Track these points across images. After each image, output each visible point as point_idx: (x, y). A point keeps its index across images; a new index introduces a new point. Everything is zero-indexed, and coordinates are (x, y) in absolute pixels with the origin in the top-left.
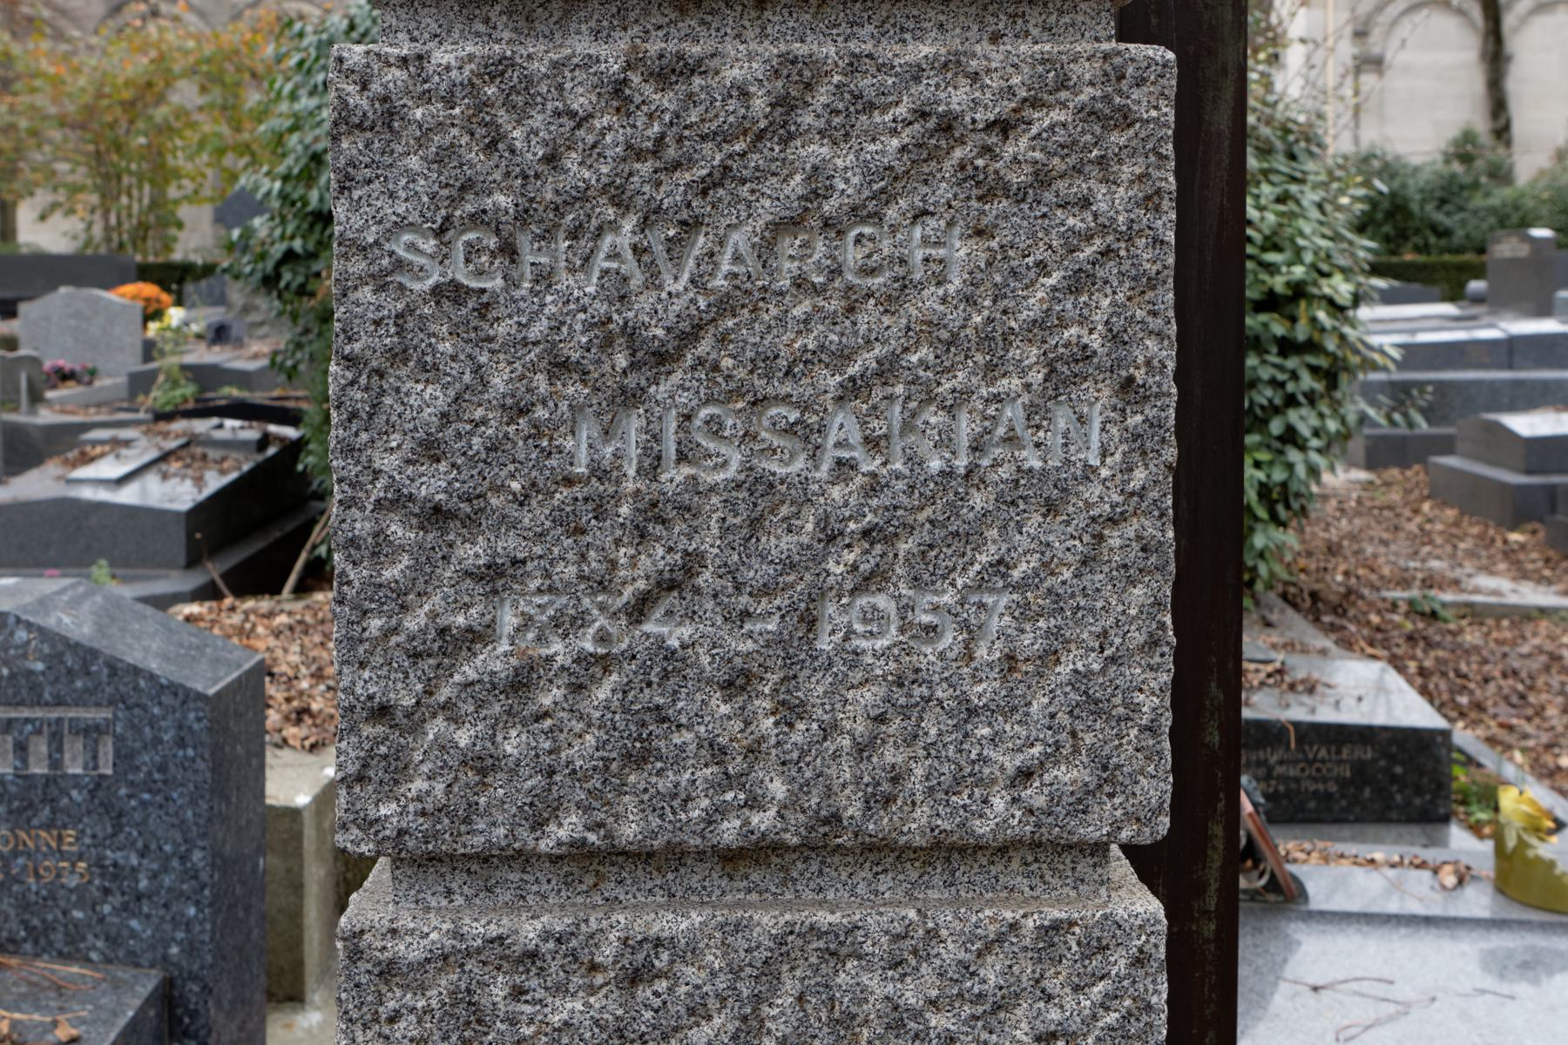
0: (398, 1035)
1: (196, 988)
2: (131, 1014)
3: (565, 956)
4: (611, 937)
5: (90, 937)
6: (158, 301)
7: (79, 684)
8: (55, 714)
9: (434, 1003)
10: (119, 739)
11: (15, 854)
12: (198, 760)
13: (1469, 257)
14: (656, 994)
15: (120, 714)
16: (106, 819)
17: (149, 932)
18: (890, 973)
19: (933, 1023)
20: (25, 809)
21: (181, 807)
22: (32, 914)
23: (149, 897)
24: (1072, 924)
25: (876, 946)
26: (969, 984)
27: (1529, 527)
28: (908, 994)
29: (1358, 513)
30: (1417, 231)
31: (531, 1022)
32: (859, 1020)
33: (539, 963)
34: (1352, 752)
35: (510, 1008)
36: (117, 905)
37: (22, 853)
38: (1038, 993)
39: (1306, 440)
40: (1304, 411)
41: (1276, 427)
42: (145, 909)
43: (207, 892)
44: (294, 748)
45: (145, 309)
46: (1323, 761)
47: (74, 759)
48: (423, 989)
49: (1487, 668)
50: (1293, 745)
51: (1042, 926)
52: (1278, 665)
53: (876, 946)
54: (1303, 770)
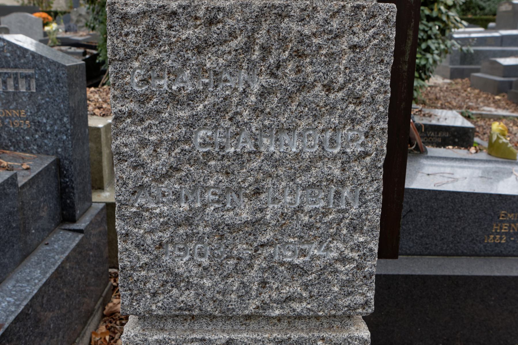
0: (128, 40)
1: (68, 162)
2: (46, 165)
3: (187, 14)
4: (203, 8)
5: (32, 145)
6: (48, 19)
7: (22, 61)
8: (15, 71)
9: (141, 30)
10: (37, 80)
11: (5, 118)
12: (64, 88)
13: (491, 17)
14: (218, 29)
15: (37, 72)
16: (34, 107)
17: (51, 144)
18: (300, 23)
19: (314, 41)
20: (7, 103)
21: (59, 103)
22: (13, 137)
23: (51, 133)
24: (364, 7)
25: (296, 13)
26: (327, 27)
27: (502, 94)
28: (306, 31)
29: (446, 91)
30: (473, 8)
31: (174, 37)
32: (288, 40)
33: (177, 17)
34: (442, 134)
35: (167, 32)
36: (40, 135)
37: (8, 118)
38: (351, 32)
39: (433, 51)
40: (434, 41)
41: (423, 46)
42: (49, 137)
43: (69, 131)
44: (97, 115)
45: (43, 21)
46: (432, 137)
47: (22, 87)
48: (136, 25)
49: (485, 131)
50: (423, 130)
51: (353, 6)
52: (420, 109)
53: (296, 13)
54: (426, 140)
